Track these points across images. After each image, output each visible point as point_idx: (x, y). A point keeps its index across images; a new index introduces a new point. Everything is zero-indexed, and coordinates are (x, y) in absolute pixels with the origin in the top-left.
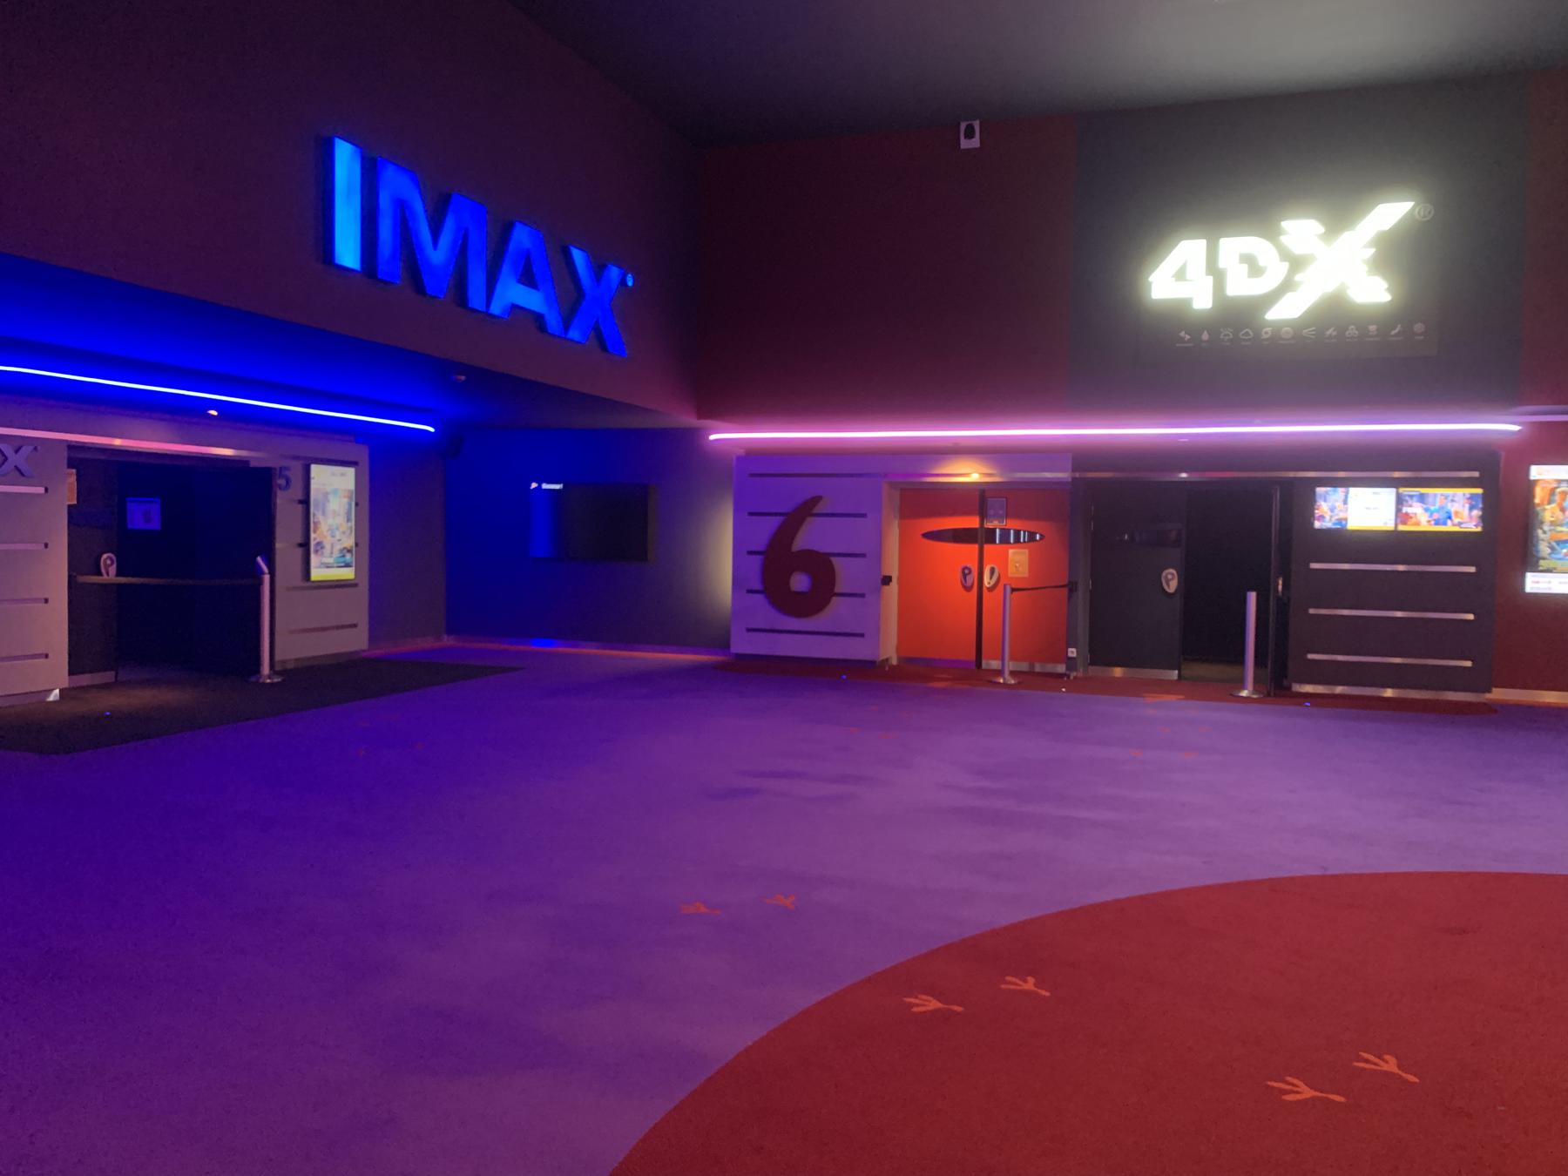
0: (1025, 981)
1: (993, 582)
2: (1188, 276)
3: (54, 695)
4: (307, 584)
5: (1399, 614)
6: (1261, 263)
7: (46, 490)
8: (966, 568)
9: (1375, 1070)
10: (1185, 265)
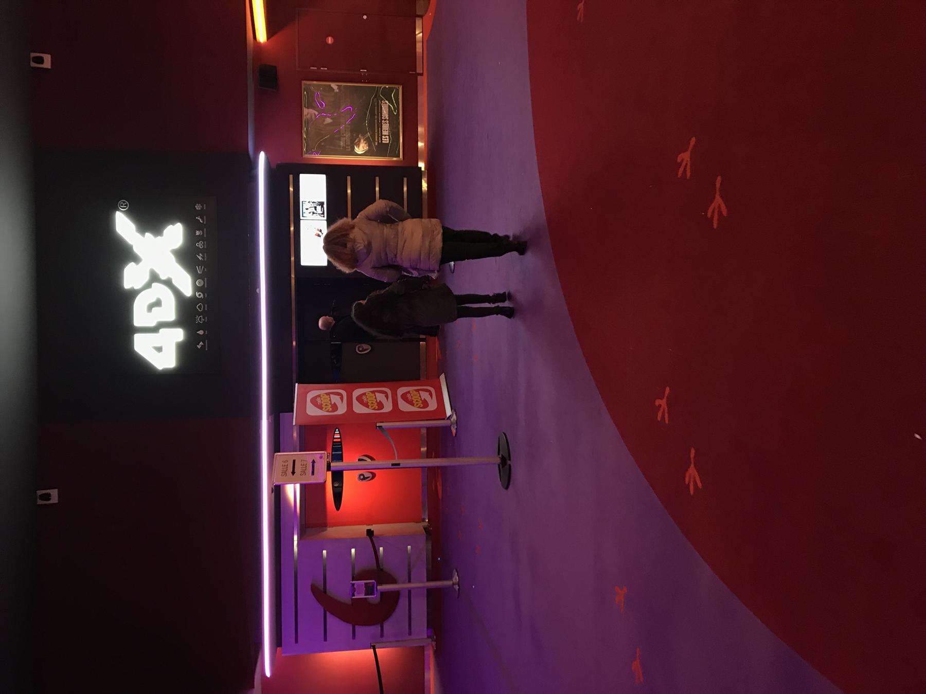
0: (660, 406)
8: (359, 478)
9: (691, 166)
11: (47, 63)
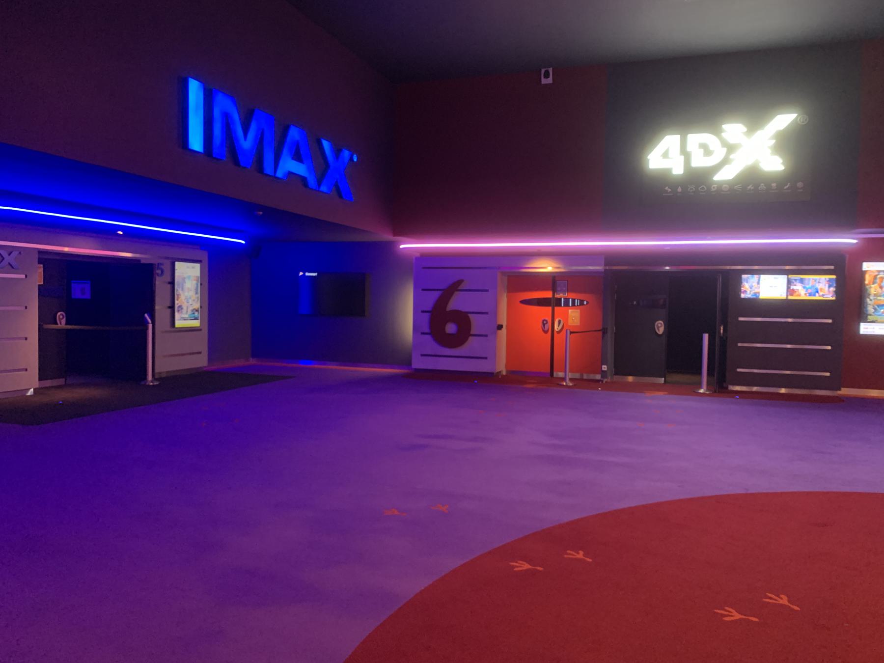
0: (578, 553)
1: (560, 328)
2: (670, 156)
3: (31, 392)
4: (173, 329)
5: (789, 346)
6: (711, 148)
7: (26, 276)
8: (545, 320)
9: (775, 603)
10: (668, 149)
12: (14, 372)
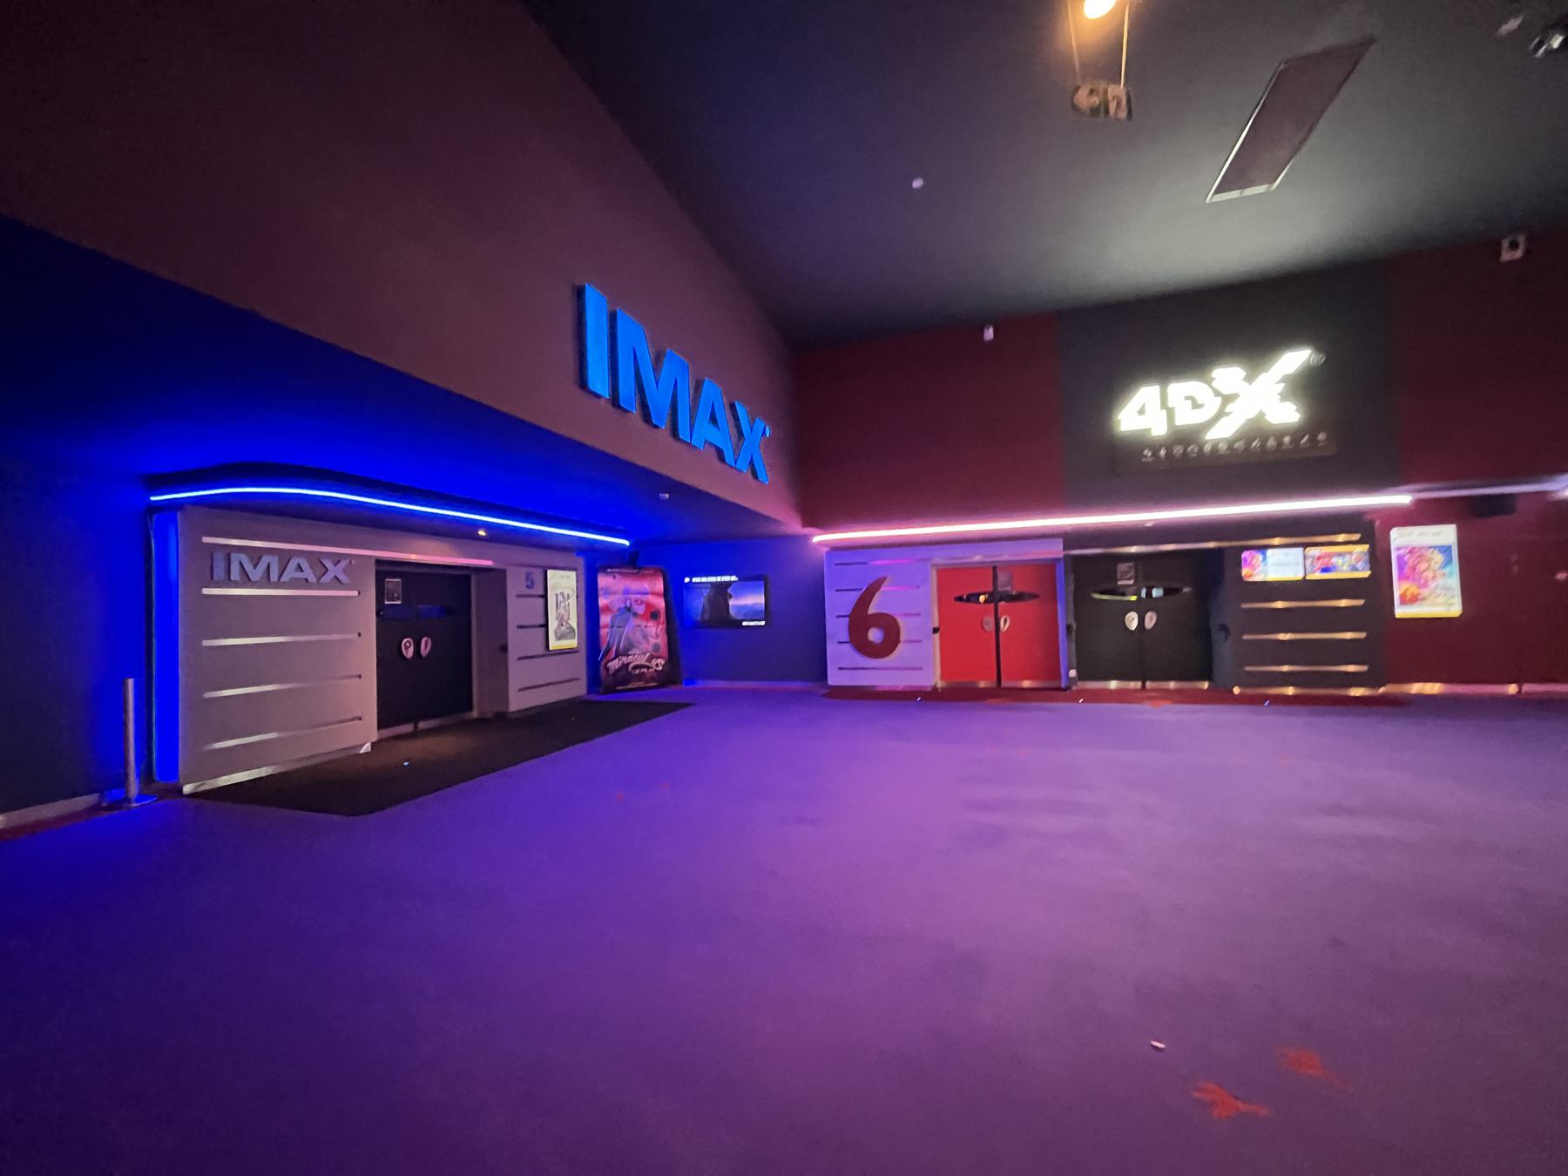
3: (366, 748)
4: (548, 653)
5: (1349, 635)
7: (359, 593)
11: (1506, 256)
12: (648, 407)
